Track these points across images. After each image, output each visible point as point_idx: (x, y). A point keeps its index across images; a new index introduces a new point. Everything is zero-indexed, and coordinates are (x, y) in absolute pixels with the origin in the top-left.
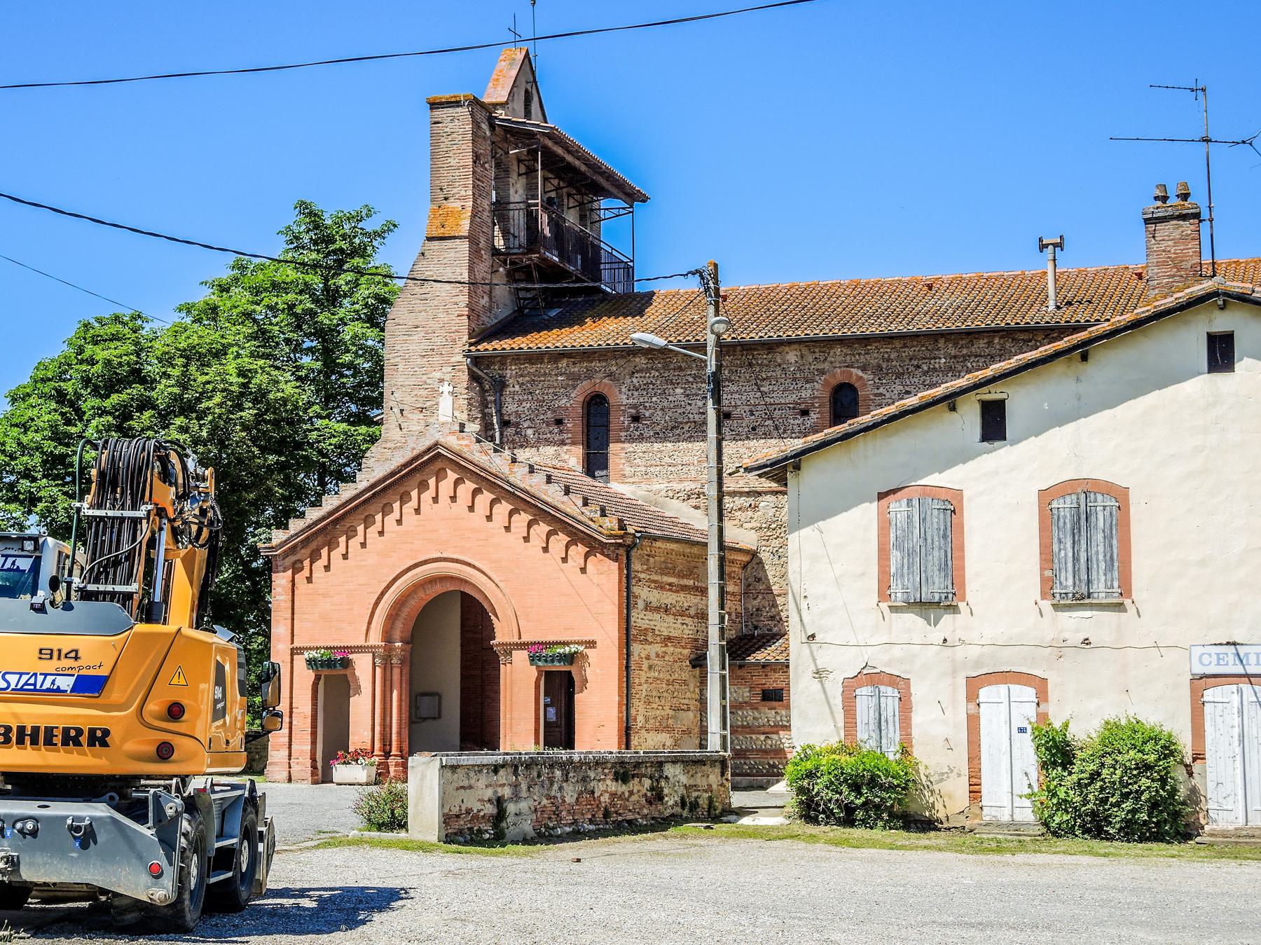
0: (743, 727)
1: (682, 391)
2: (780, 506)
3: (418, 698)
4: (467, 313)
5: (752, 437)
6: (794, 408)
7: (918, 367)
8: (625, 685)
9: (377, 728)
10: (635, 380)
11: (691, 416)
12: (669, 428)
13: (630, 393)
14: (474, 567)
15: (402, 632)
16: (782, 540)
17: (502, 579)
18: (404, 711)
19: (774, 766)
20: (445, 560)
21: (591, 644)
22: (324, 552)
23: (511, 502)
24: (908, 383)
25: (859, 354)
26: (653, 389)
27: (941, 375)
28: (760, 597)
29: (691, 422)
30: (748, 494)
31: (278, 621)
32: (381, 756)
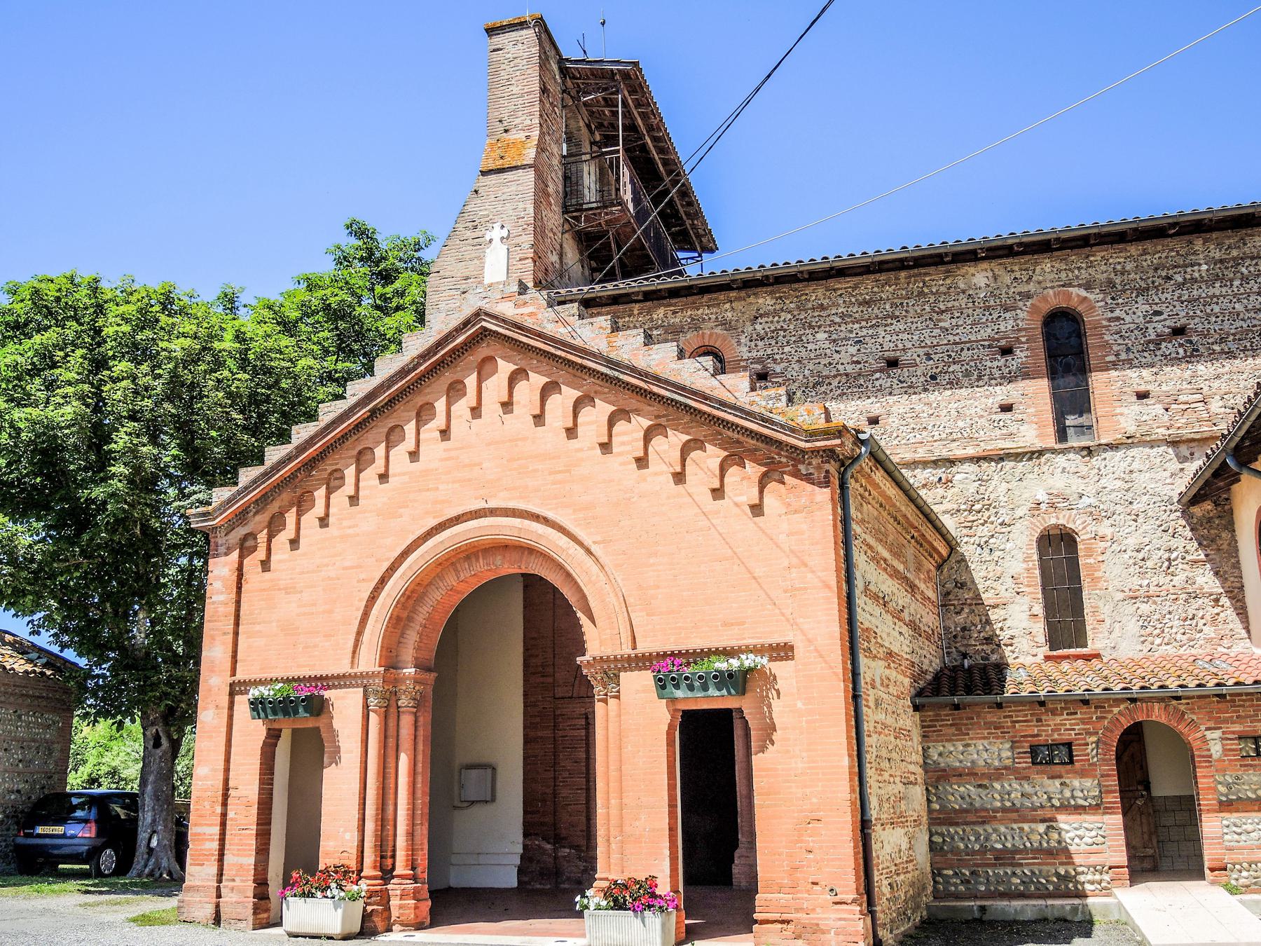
0: (1004, 810)
1: (826, 335)
2: (985, 478)
3: (463, 771)
4: (532, 255)
5: (932, 388)
6: (990, 346)
7: (1168, 278)
8: (854, 734)
9: (370, 826)
10: (758, 327)
11: (840, 367)
12: (811, 385)
13: (753, 344)
14: (546, 521)
15: (418, 649)
16: (993, 526)
17: (599, 538)
18: (419, 794)
19: (1066, 878)
20: (493, 512)
21: (783, 652)
22: (291, 517)
23: (613, 398)
24: (1157, 301)
25: (1079, 268)
26: (784, 337)
27: (1204, 287)
28: (966, 610)
29: (841, 375)
30: (935, 463)
31: (213, 638)
32: (374, 878)
